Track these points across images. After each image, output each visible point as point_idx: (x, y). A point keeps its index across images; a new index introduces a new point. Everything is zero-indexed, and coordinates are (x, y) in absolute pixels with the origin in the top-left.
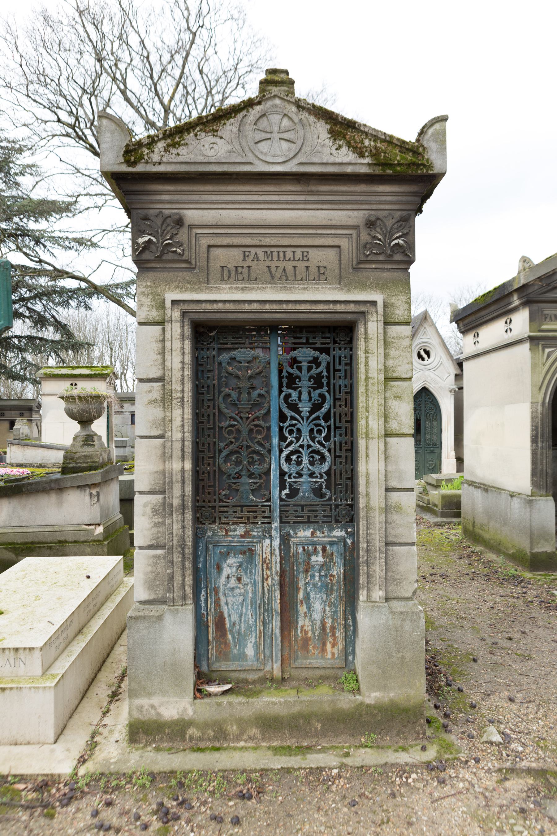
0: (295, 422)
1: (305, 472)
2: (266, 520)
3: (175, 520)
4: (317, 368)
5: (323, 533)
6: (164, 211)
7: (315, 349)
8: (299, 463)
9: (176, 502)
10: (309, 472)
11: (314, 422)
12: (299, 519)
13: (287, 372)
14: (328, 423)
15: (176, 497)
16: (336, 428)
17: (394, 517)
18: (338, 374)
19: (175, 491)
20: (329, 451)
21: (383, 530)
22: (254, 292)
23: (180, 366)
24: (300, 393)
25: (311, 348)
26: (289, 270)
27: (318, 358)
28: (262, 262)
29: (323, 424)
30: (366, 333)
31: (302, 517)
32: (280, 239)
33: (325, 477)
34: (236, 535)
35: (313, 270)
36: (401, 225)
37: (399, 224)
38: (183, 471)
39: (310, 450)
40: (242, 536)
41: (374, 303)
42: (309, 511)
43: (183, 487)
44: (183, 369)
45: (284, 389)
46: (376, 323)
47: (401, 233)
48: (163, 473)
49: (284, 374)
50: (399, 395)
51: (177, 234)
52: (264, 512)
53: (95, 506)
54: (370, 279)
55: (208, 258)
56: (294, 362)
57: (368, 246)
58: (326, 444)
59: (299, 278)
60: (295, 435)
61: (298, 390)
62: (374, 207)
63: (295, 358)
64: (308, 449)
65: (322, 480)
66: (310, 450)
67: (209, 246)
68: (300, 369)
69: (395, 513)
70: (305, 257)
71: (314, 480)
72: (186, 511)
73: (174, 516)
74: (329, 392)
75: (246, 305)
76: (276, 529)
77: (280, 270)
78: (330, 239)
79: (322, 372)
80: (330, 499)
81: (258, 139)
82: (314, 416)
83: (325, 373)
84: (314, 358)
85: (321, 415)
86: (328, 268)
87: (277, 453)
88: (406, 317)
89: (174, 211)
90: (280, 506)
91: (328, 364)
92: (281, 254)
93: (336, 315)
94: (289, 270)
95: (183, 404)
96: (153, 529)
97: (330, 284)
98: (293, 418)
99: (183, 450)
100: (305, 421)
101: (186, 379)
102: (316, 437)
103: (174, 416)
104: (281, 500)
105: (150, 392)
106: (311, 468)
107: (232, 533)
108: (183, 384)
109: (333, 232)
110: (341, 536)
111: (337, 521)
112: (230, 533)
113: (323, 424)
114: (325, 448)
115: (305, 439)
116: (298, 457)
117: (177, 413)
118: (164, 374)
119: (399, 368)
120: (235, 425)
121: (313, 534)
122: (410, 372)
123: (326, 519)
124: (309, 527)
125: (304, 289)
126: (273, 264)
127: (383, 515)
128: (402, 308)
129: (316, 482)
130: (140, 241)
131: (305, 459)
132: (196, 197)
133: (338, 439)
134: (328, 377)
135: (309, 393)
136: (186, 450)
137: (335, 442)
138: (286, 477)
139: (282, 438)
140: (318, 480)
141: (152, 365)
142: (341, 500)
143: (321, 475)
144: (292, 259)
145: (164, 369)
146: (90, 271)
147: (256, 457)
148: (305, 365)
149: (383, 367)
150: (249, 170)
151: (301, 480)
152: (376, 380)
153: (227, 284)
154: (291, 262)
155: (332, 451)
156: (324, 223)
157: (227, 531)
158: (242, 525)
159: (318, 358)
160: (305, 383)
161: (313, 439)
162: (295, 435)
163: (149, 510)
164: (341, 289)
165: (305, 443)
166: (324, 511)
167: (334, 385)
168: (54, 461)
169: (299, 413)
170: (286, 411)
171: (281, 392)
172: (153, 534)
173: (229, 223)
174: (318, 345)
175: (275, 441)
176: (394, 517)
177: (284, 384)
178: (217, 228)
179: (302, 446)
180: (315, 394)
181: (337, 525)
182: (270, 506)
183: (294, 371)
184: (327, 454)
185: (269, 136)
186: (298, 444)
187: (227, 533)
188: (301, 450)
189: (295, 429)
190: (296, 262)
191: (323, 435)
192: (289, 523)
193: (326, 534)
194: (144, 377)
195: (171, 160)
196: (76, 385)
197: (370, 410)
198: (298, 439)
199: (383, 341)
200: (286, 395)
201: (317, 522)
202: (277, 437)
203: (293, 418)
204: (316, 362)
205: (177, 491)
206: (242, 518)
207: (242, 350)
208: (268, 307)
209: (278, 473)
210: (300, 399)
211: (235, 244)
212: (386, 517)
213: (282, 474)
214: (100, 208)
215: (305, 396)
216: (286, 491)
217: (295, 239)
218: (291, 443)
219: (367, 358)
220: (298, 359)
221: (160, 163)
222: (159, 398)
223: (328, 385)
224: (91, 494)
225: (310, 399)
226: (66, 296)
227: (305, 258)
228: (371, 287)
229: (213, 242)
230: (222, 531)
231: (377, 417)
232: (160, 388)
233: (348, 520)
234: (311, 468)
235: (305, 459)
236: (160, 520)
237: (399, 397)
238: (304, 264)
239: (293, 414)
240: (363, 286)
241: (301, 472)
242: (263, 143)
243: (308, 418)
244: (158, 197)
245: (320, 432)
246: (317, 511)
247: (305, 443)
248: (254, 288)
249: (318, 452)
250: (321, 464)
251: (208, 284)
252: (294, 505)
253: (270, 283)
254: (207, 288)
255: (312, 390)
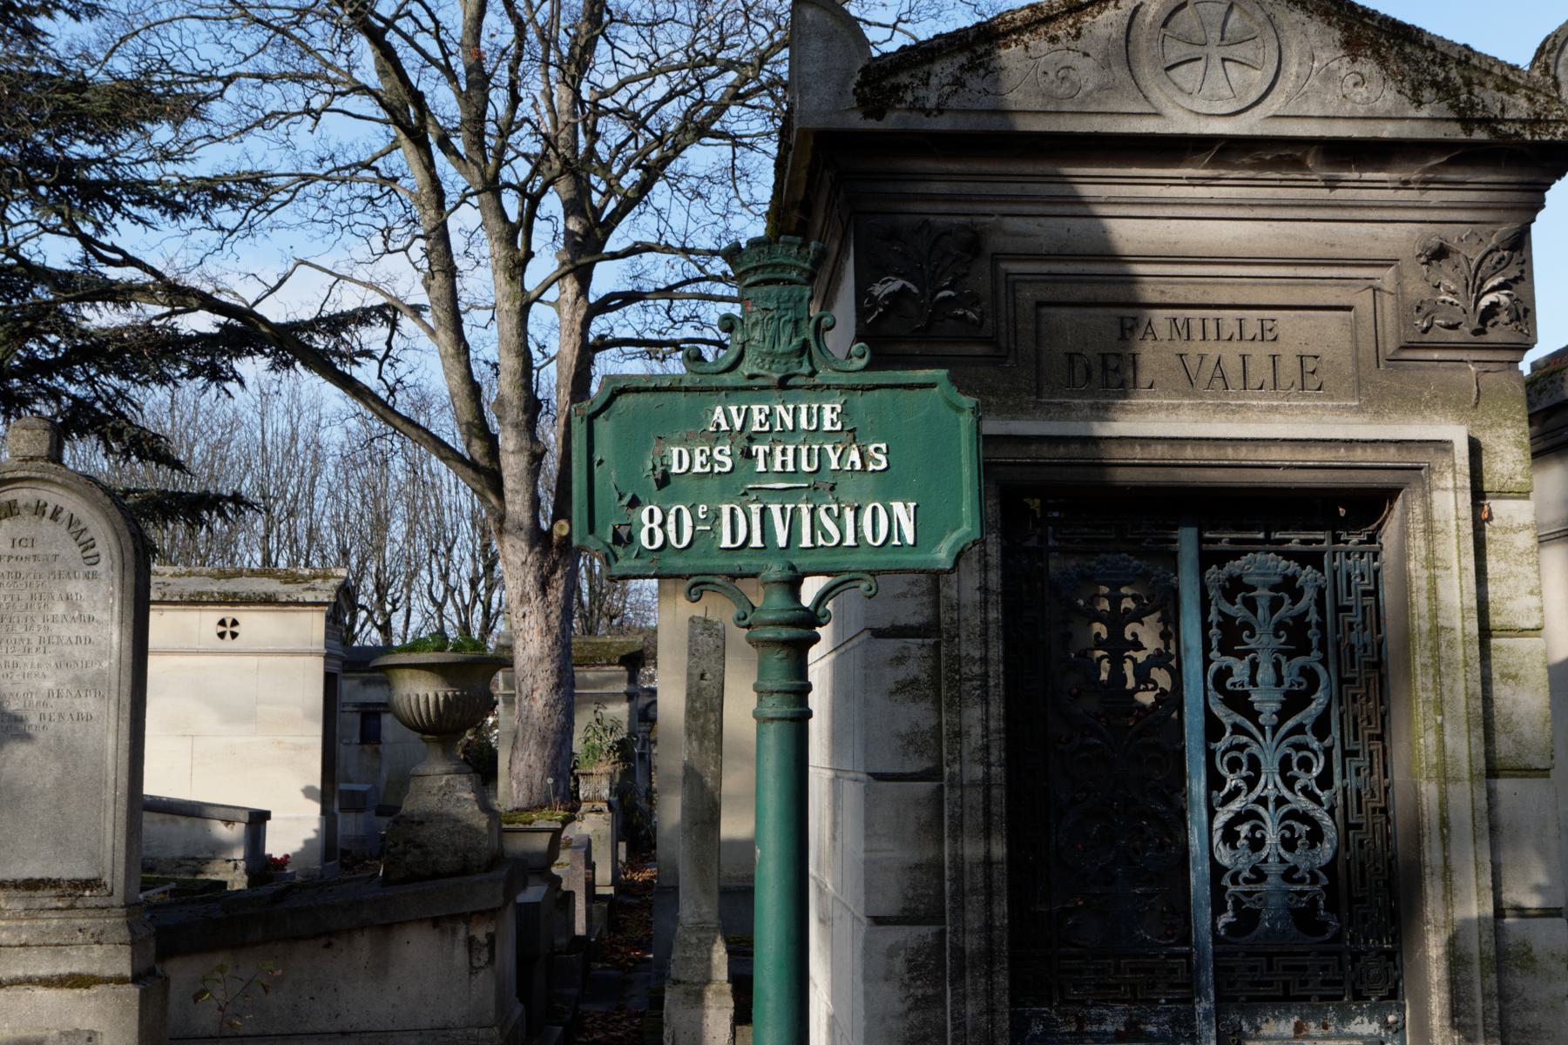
0: (1244, 739)
1: (1273, 868)
2: (1179, 993)
3: (969, 989)
4: (1294, 603)
5: (1325, 1027)
6: (932, 218)
7: (1288, 555)
8: (1256, 844)
9: (972, 943)
10: (1284, 867)
11: (1293, 739)
12: (1263, 991)
13: (1220, 612)
14: (1327, 742)
15: (971, 932)
16: (1346, 754)
17: (1518, 981)
18: (1347, 618)
19: (969, 916)
20: (1331, 812)
21: (1495, 1015)
22: (1162, 415)
23: (978, 596)
24: (1254, 666)
25: (1278, 553)
26: (1232, 365)
27: (1294, 578)
28: (1165, 343)
29: (1315, 745)
30: (1428, 518)
31: (1270, 984)
32: (1208, 288)
33: (1324, 880)
34: (1105, 1033)
35: (1289, 366)
36: (1502, 259)
37: (1496, 256)
38: (988, 862)
39: (1284, 809)
40: (1119, 1036)
41: (1443, 446)
42: (1286, 968)
43: (988, 904)
44: (984, 605)
45: (1214, 654)
46: (1452, 495)
47: (1501, 279)
48: (936, 867)
49: (1213, 617)
50: (1513, 671)
51: (966, 275)
52: (1174, 971)
53: (481, 975)
54: (1428, 387)
55: (1037, 331)
56: (1234, 588)
57: (1426, 308)
58: (1324, 796)
59: (1254, 381)
60: (1244, 772)
61: (1247, 659)
62: (1435, 215)
63: (1240, 577)
64: (1277, 807)
65: (1317, 888)
66: (1284, 809)
67: (1040, 304)
68: (1251, 605)
69: (1518, 972)
70: (1266, 334)
71: (1298, 888)
72: (997, 968)
73: (968, 980)
74: (1324, 662)
75: (1138, 449)
76: (1206, 1017)
77: (1210, 364)
78: (1328, 290)
79: (1306, 613)
80: (1338, 937)
81: (1173, 58)
82: (1290, 723)
83: (1313, 617)
84: (1285, 577)
85: (1309, 722)
86: (1326, 358)
87: (1205, 818)
88: (1519, 479)
89: (955, 220)
90: (1215, 954)
91: (1321, 592)
92: (1211, 326)
93: (1353, 472)
94: (1232, 365)
95: (987, 693)
96: (912, 1016)
97: (1332, 398)
98: (1238, 730)
99: (987, 812)
100: (1268, 736)
101: (992, 632)
102: (1296, 778)
103: (966, 722)
104: (1217, 939)
105: (900, 660)
106: (1287, 856)
107: (1095, 1028)
108: (986, 643)
109: (1335, 272)
110: (1371, 1036)
111: (1358, 997)
112: (1088, 1028)
113: (1315, 745)
114: (1321, 804)
115: (1270, 783)
116: (1254, 829)
117: (973, 715)
118: (937, 616)
119: (1509, 604)
120: (1246, 745)
121: (1299, 1028)
122: (1536, 614)
123: (1328, 991)
124: (1288, 1010)
125: (1272, 409)
126: (1195, 348)
127: (1494, 977)
128: (1509, 457)
129: (1301, 893)
130: (879, 290)
131: (1272, 835)
132: (1014, 189)
133: (1352, 781)
134: (1322, 626)
135: (1277, 666)
136: (994, 809)
137: (1345, 789)
138: (1226, 881)
139: (1215, 781)
140: (1307, 888)
141: (904, 595)
142: (1366, 942)
143: (1311, 873)
144: (1237, 336)
145: (936, 605)
146: (260, 290)
147: (1302, 828)
148: (1263, 595)
149: (1474, 604)
150: (1152, 130)
151: (1263, 887)
152: (1459, 634)
153: (1082, 395)
154: (1235, 344)
155: (1337, 812)
156: (1314, 253)
157: (1080, 1022)
158: (1119, 1007)
159: (1294, 578)
160: (1263, 642)
161: (1289, 783)
162: (1244, 772)
163: (899, 964)
164: (1359, 410)
165: (1271, 793)
166: (1325, 968)
167: (1338, 644)
168: (178, 853)
169: (1253, 715)
170: (1220, 711)
171: (1207, 662)
172: (910, 1029)
173: (1089, 251)
174: (1294, 545)
175: (1197, 786)
176: (1518, 981)
177: (1214, 643)
178: (1059, 261)
179: (1262, 801)
180: (1290, 669)
181: (1360, 1006)
182: (1188, 956)
183: (1237, 610)
184: (1327, 821)
185: (1196, 51)
186: (1253, 796)
187: (1080, 1027)
188: (1261, 810)
189: (1244, 760)
190: (1250, 344)
191: (1316, 771)
192: (1235, 999)
193: (1332, 1029)
194: (884, 623)
195: (969, 106)
196: (235, 623)
197: (1446, 709)
198: (1252, 783)
199: (1471, 539)
200: (1220, 670)
201: (1307, 998)
202: (1203, 778)
203: (1238, 730)
204: (1289, 586)
205: (974, 918)
206: (1117, 986)
207: (1110, 557)
208: (1189, 453)
209: (1208, 871)
210: (1253, 682)
211: (1101, 299)
212: (1499, 982)
213: (1217, 870)
214: (316, 115)
215: (1265, 674)
216: (1226, 918)
217: (1246, 290)
218: (1235, 792)
219: (1433, 580)
220: (1246, 580)
221: (941, 112)
222: (923, 676)
223: (1322, 646)
224: (471, 942)
225: (1279, 681)
226: (154, 353)
227: (1269, 336)
228: (1430, 405)
229: (1046, 295)
230: (1068, 1023)
231: (1465, 727)
232: (925, 652)
233: (1384, 993)
234: (1287, 856)
235: (1272, 835)
236: (930, 992)
237: (1515, 677)
238: (1267, 349)
239: (1239, 719)
240: (1412, 403)
241: (1264, 867)
242: (1184, 68)
243: (1275, 729)
244: (922, 188)
245: (1306, 765)
246: (1304, 968)
247: (1271, 793)
248: (1150, 407)
249: (1304, 817)
250: (1313, 846)
251: (1039, 394)
252: (1249, 954)
253: (1187, 395)
254: (1038, 405)
255: (1283, 659)
